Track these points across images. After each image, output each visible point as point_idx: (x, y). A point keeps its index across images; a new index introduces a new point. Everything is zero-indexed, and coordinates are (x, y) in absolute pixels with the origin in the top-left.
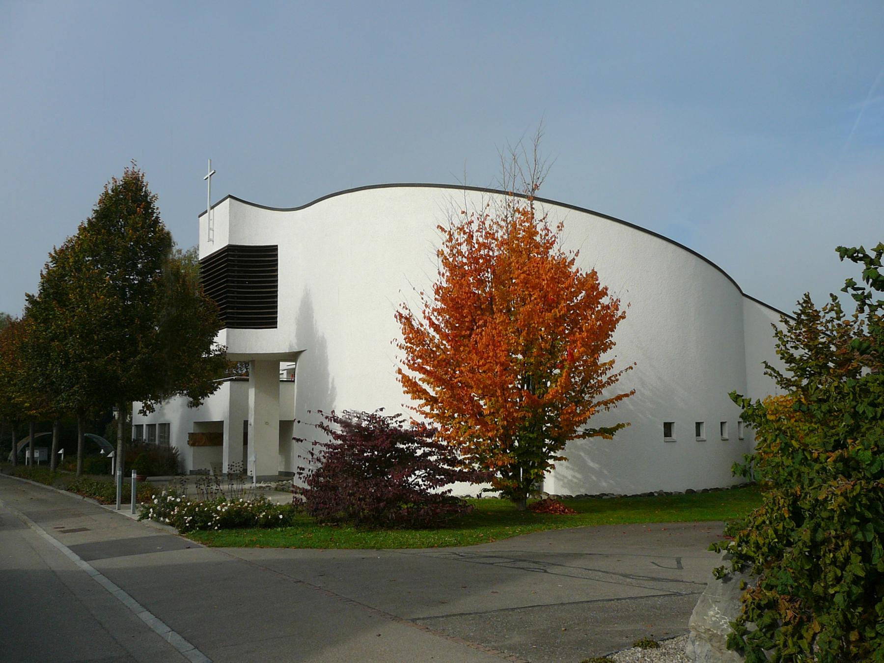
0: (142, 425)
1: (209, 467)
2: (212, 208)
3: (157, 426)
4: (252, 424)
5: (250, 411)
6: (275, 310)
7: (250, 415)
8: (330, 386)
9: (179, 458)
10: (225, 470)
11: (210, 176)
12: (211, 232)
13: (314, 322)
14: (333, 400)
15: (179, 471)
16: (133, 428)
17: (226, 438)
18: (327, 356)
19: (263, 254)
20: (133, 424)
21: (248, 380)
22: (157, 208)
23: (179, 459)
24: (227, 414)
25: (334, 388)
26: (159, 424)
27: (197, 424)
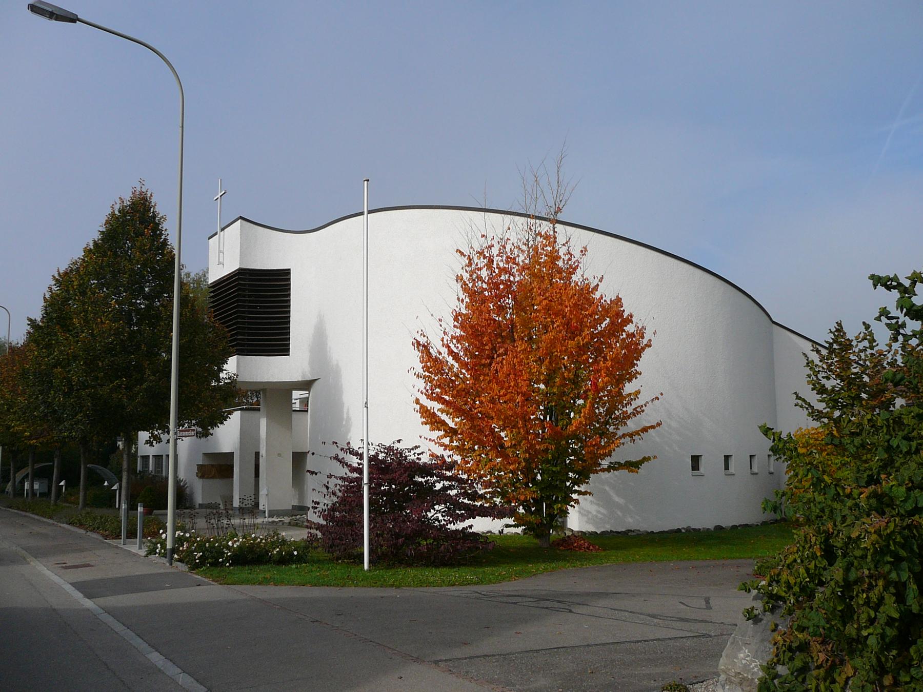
2: (223, 230)
5: (261, 442)
7: (261, 446)
8: (345, 416)
10: (236, 504)
11: (221, 196)
12: (221, 254)
13: (328, 349)
16: (139, 459)
18: (342, 385)
21: (259, 410)
24: (237, 445)
25: (349, 419)
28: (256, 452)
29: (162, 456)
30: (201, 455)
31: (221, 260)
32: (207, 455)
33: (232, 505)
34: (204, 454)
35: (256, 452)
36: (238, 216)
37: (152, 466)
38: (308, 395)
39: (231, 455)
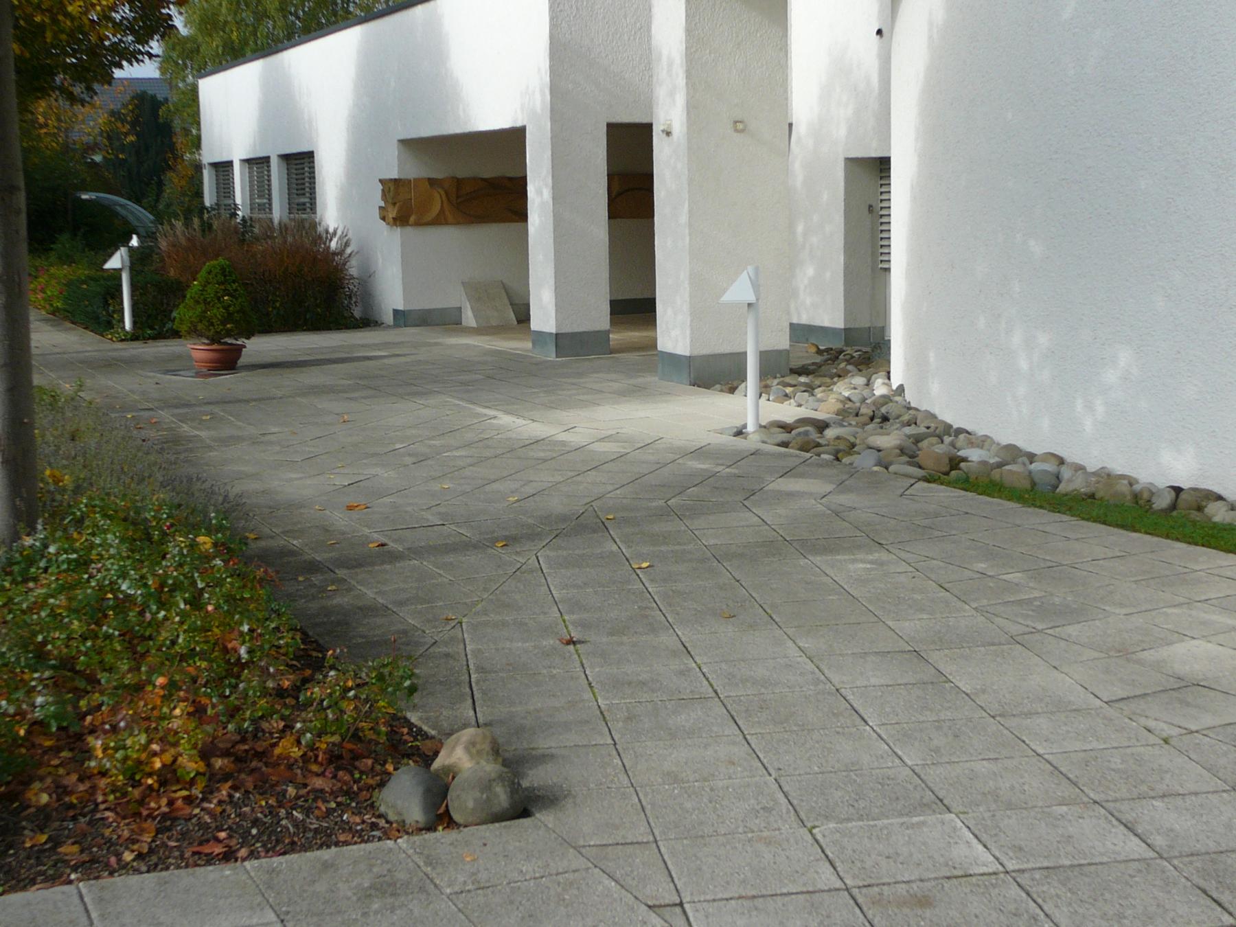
0: (229, 164)
3: (275, 163)
5: (661, 73)
7: (661, 93)
9: (353, 269)
10: (544, 317)
17: (539, 193)
28: (614, 130)
29: (266, 160)
32: (414, 146)
35: (614, 130)
37: (242, 180)
39: (514, 139)
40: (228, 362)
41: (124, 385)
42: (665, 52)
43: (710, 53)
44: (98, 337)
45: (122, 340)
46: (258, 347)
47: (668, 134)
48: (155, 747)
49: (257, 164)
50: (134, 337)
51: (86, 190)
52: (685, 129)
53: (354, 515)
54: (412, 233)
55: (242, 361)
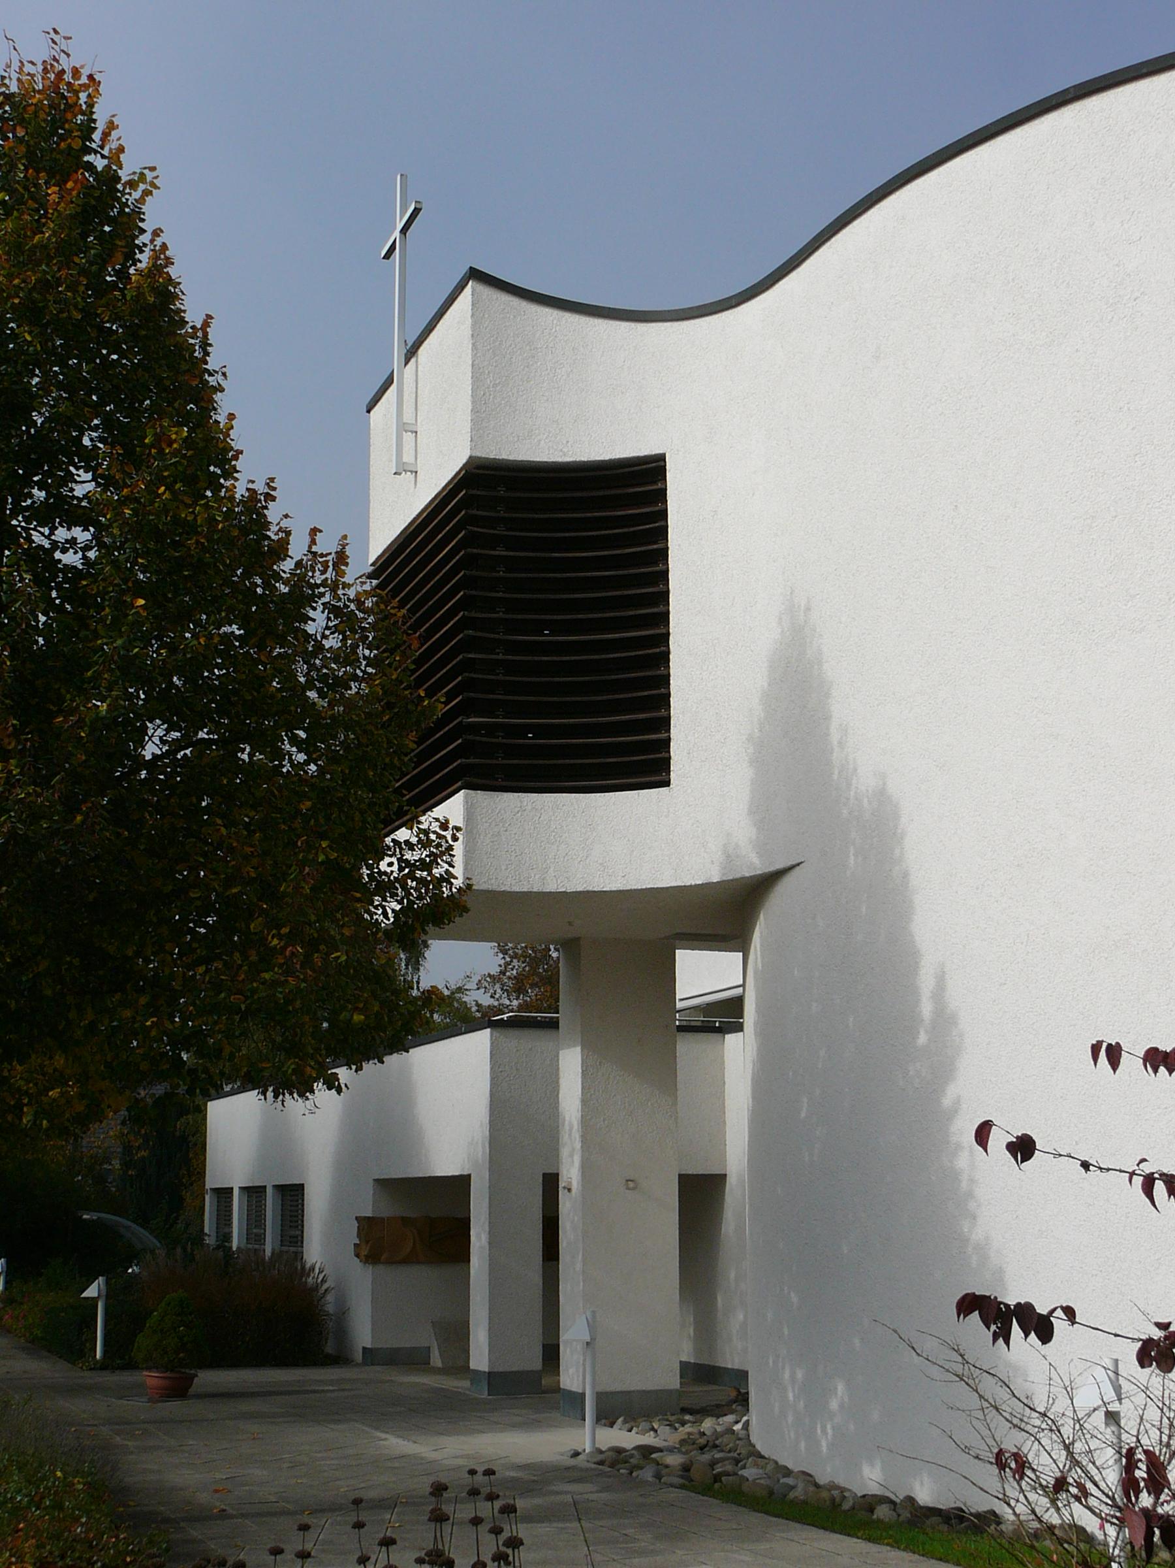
0: (230, 1190)
1: (424, 1337)
2: (411, 353)
3: (269, 1191)
4: (575, 1186)
5: (565, 1137)
6: (664, 736)
7: (564, 1152)
8: (926, 1009)
9: (330, 1304)
10: (480, 1359)
11: (404, 230)
12: (408, 437)
13: (835, 737)
14: (943, 1071)
15: (329, 1348)
16: (207, 1198)
17: (478, 1236)
18: (906, 875)
19: (613, 492)
20: (207, 1187)
21: (553, 1025)
22: (157, 233)
23: (330, 1308)
24: (482, 1152)
25: (944, 1020)
26: (276, 1187)
27: (386, 1185)
30: (371, 1182)
31: (408, 458)
33: (485, 1372)
34: (378, 1181)
36: (464, 270)
38: (740, 990)
39: (462, 1183)
40: (179, 1390)
41: (79, 1407)
42: (567, 1118)
43: (604, 1121)
44: (70, 1365)
45: (91, 1369)
46: (207, 1379)
47: (569, 1190)
48: (13, 1559)
49: (254, 1193)
50: (104, 1366)
51: (88, 1210)
52: (580, 1188)
53: (217, 1495)
54: (381, 1269)
55: (192, 1391)
